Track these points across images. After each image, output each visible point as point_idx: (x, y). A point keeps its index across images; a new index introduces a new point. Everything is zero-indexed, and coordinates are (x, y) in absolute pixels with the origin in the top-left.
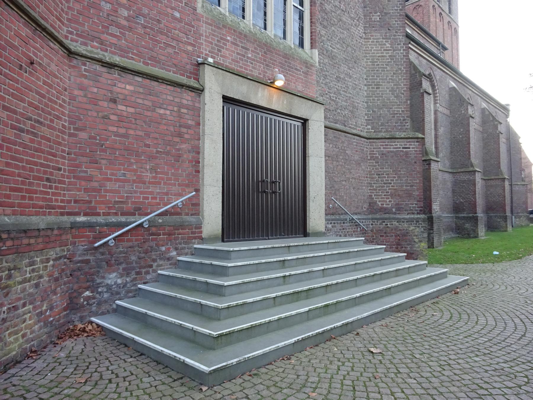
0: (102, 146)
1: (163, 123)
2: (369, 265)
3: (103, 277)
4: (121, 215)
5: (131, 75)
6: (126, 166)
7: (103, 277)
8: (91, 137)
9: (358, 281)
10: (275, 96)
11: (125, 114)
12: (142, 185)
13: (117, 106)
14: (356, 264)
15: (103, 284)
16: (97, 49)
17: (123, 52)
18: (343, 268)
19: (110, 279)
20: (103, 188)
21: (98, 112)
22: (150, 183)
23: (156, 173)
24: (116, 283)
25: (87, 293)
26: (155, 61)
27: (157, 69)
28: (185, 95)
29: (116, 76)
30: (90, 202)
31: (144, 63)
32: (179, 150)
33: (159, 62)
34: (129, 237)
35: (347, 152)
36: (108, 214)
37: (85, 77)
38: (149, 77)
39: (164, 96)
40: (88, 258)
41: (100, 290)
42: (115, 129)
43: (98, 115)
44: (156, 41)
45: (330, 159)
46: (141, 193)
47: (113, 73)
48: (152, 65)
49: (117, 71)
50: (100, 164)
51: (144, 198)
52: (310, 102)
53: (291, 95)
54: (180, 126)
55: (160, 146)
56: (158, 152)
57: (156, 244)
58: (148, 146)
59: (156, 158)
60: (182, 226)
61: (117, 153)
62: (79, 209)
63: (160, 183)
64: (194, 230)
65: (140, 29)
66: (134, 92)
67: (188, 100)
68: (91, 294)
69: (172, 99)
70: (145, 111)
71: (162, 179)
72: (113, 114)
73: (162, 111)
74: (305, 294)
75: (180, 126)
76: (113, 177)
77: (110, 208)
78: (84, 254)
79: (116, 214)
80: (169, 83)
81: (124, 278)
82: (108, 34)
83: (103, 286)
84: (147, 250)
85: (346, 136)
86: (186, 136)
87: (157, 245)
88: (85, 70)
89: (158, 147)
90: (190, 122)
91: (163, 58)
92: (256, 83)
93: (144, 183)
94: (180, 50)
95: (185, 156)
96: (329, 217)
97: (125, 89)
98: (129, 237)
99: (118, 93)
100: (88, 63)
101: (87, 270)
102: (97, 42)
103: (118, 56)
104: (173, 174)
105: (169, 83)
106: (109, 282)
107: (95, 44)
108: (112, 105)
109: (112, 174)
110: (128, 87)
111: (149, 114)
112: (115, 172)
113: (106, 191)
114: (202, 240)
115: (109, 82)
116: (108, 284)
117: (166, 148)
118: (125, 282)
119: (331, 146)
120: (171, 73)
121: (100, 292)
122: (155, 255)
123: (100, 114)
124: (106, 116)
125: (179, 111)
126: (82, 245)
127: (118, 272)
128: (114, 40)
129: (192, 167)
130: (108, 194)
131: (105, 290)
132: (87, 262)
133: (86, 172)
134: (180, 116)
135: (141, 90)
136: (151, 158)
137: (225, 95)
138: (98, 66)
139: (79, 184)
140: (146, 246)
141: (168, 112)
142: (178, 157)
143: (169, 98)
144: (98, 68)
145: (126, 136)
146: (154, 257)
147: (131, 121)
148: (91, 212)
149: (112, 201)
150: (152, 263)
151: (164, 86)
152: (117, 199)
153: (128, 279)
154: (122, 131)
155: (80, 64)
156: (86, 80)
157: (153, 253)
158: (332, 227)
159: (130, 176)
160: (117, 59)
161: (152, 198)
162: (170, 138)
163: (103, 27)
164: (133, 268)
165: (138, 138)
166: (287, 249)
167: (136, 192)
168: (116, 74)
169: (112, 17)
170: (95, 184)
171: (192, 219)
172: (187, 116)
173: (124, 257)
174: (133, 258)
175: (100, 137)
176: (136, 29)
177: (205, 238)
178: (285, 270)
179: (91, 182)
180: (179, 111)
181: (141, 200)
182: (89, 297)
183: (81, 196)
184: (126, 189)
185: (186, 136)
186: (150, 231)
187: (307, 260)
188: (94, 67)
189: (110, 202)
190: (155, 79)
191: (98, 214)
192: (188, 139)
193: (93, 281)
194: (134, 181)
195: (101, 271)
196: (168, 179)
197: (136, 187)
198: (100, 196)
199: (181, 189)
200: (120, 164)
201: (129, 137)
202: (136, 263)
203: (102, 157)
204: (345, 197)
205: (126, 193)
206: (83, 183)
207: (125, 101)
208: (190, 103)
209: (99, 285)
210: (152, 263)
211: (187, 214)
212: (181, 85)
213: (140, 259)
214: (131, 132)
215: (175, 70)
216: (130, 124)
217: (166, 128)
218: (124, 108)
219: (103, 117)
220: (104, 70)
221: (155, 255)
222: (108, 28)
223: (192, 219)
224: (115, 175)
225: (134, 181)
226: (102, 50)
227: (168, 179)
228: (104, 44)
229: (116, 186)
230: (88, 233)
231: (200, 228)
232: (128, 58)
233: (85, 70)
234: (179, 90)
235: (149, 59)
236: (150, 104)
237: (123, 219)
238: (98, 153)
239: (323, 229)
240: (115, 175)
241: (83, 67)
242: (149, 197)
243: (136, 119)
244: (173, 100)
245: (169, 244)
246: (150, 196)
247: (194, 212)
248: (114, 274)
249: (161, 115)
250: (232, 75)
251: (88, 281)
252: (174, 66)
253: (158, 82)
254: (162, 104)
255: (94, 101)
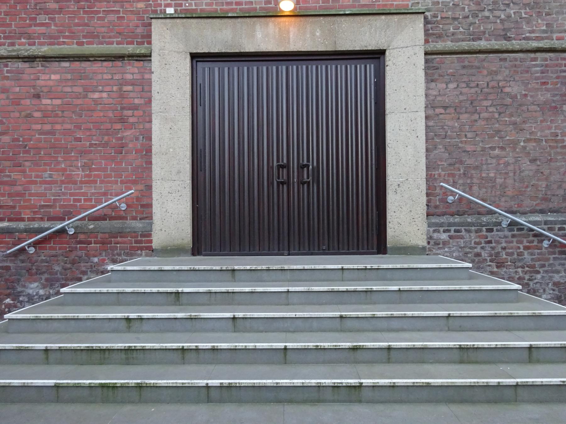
0: (25, 147)
1: (99, 109)
2: (395, 324)
3: (24, 286)
4: (47, 220)
5: (57, 63)
6: (53, 166)
7: (24, 286)
8: (14, 140)
9: (188, 355)
10: (291, 29)
11: (50, 108)
12: (73, 186)
13: (41, 101)
14: (449, 316)
15: (24, 294)
16: (25, 45)
17: (53, 39)
18: (299, 322)
19: (32, 289)
20: (27, 192)
21: (20, 112)
22: (82, 182)
23: (91, 170)
24: (37, 294)
25: (8, 301)
26: (92, 36)
27: (95, 46)
28: (128, 68)
29: (40, 68)
30: (14, 207)
31: (79, 44)
32: (121, 139)
33: (97, 37)
34: (52, 245)
35: (507, 90)
36: (33, 219)
37: (7, 78)
38: (76, 59)
39: (100, 77)
40: (8, 265)
41: (21, 299)
42: (39, 127)
43: (20, 114)
44: (92, 12)
45: (451, 110)
46: (71, 194)
47: (36, 66)
48: (89, 43)
49: (40, 63)
50: (24, 166)
51: (75, 200)
52: (383, 17)
53: (329, 19)
54: (123, 108)
55: (94, 138)
56: (91, 145)
57: (85, 254)
58: (79, 140)
59: (90, 152)
60: (121, 233)
61: (42, 153)
62: (3, 214)
63: (95, 182)
64: (139, 238)
65: (72, 7)
66: (60, 81)
67: (133, 74)
68: (12, 302)
69: (110, 77)
70: (74, 100)
71: (98, 176)
72: (36, 111)
73: (96, 95)
74: (123, 356)
75: (123, 108)
76: (38, 179)
77: (35, 213)
78: (4, 261)
79: (42, 219)
80: (103, 59)
81: (48, 289)
82: (36, 25)
83: (24, 295)
84: (74, 260)
85: (501, 60)
86: (131, 120)
87: (87, 255)
88: (8, 72)
89: (92, 139)
90: (137, 101)
91: (104, 29)
92: (248, 20)
93: (75, 183)
94: (125, 12)
95: (130, 145)
96: (434, 220)
97: (50, 79)
98: (52, 245)
99: (41, 87)
100: (9, 63)
101: (7, 277)
102: (24, 38)
103: (48, 45)
104: (112, 170)
105: (103, 59)
106: (30, 291)
107: (23, 40)
108: (35, 101)
109: (37, 176)
110: (53, 77)
111: (79, 102)
112: (40, 173)
113: (30, 195)
114: (151, 251)
115: (32, 77)
116: (29, 294)
117: (103, 138)
118: (47, 293)
119: (452, 86)
120: (115, 45)
121: (22, 301)
122: (84, 266)
123: (23, 113)
124: (30, 114)
125: (120, 89)
126: (2, 252)
127: (40, 283)
128: (43, 29)
129: (142, 158)
130: (33, 198)
131: (26, 300)
132: (8, 268)
133: (9, 176)
134: (122, 95)
135: (69, 76)
136: (83, 153)
137: (194, 51)
138: (20, 64)
139: (4, 189)
140: (73, 256)
141: (105, 95)
142: (120, 148)
143: (105, 77)
144: (20, 65)
145: (52, 133)
146: (84, 269)
147: (57, 114)
148: (15, 218)
149: (37, 205)
150: (81, 276)
151: (99, 64)
152: (42, 203)
153: (51, 291)
154: (47, 127)
155: (2, 66)
156: (9, 81)
157: (82, 264)
158: (451, 237)
159: (57, 176)
160: (45, 50)
161: (85, 200)
162: (108, 126)
163: (31, 19)
164: (58, 280)
165: (66, 132)
166: (230, 274)
167: (64, 194)
168: (39, 66)
169: (40, 5)
170: (19, 188)
171: (138, 225)
172: (131, 95)
173: (48, 266)
174: (57, 268)
175: (23, 138)
176: (68, 8)
177: (155, 249)
178: (178, 307)
179: (15, 187)
180: (120, 89)
181: (72, 203)
182: (10, 304)
183: (5, 201)
184: (53, 191)
185: (131, 120)
186: (82, 238)
187: (236, 297)
188: (16, 65)
189: (35, 207)
190: (85, 59)
191: (22, 220)
192: (133, 124)
193: (13, 288)
194: (63, 182)
195: (22, 280)
196: (107, 176)
197: (65, 188)
198: (25, 201)
199: (125, 187)
200: (45, 164)
201: (55, 132)
202: (61, 274)
203: (25, 159)
204: (499, 181)
205: (54, 196)
206: (7, 188)
207: (51, 94)
208: (137, 76)
209: (19, 294)
210: (81, 276)
211: (134, 218)
212: (121, 57)
213: (65, 269)
214: (58, 127)
215: (120, 39)
216: (56, 119)
217: (102, 114)
218: (49, 101)
219: (27, 116)
220: (27, 65)
221: (84, 266)
222: (35, 18)
223: (138, 225)
224: (41, 177)
225: (63, 182)
226: (29, 45)
227: (107, 176)
228: (32, 37)
229: (41, 189)
230: (7, 240)
231: (150, 235)
232: (59, 44)
233: (8, 72)
234: (119, 63)
235: (84, 37)
236: (80, 90)
237: (46, 224)
238: (21, 155)
239: (421, 241)
240: (41, 177)
241: (5, 69)
242: (81, 199)
243: (63, 111)
244: (112, 79)
245: (104, 254)
246: (83, 198)
247: (145, 216)
248: (35, 285)
249: (95, 100)
250: (199, 20)
251: (8, 288)
252: (118, 35)
253: (90, 61)
254: (97, 87)
255: (16, 102)
